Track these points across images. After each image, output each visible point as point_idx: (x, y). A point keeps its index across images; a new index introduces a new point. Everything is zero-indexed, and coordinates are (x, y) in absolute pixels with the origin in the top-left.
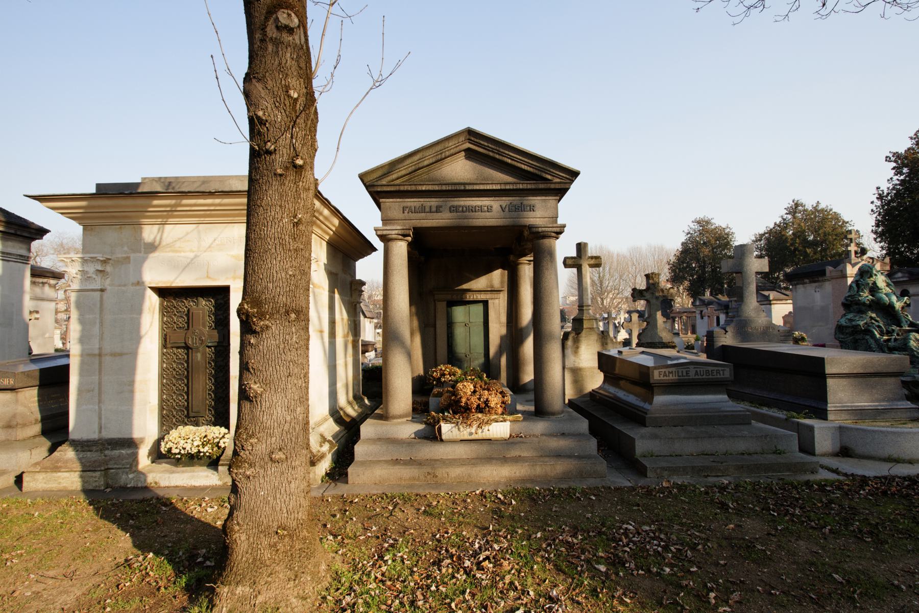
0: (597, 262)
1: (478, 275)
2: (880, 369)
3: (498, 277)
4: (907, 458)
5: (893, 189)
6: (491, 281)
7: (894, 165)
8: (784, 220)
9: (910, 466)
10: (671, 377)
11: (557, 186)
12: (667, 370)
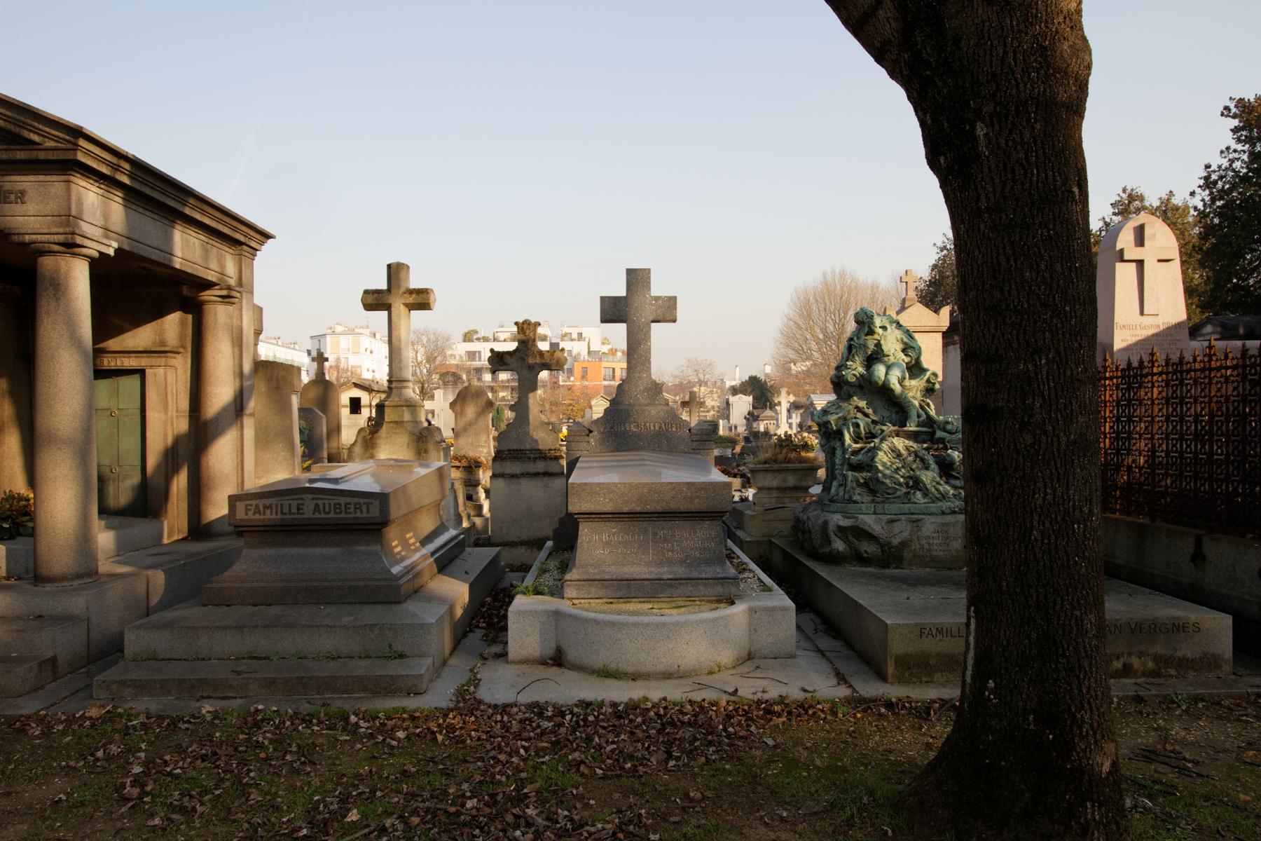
0: (421, 300)
1: (137, 322)
2: (673, 506)
3: (173, 325)
4: (631, 670)
5: (1230, 168)
6: (161, 333)
7: (1236, 122)
8: (1107, 224)
9: (631, 683)
10: (268, 515)
11: (52, 156)
12: (261, 503)
